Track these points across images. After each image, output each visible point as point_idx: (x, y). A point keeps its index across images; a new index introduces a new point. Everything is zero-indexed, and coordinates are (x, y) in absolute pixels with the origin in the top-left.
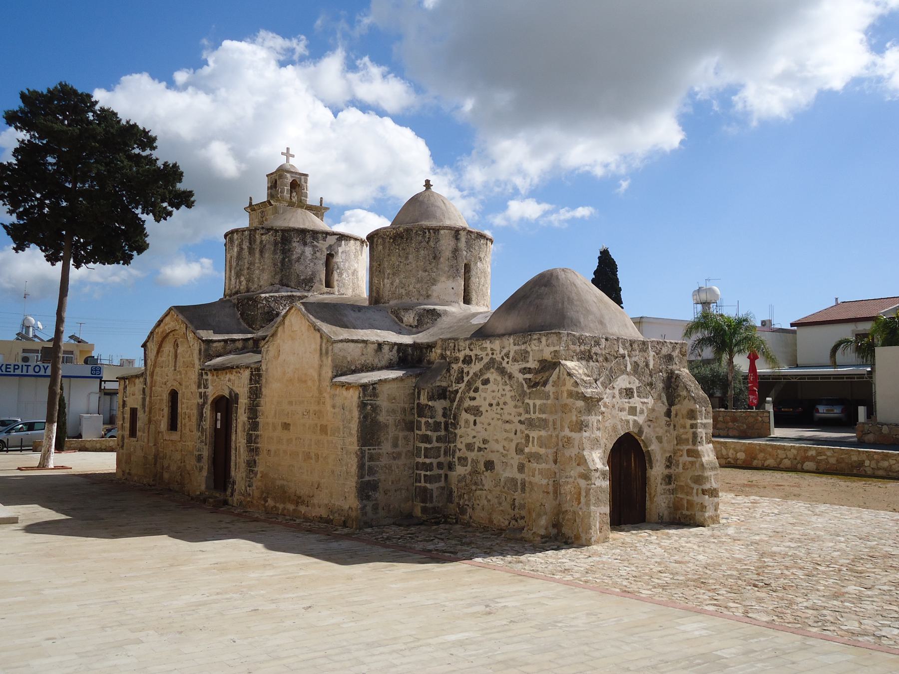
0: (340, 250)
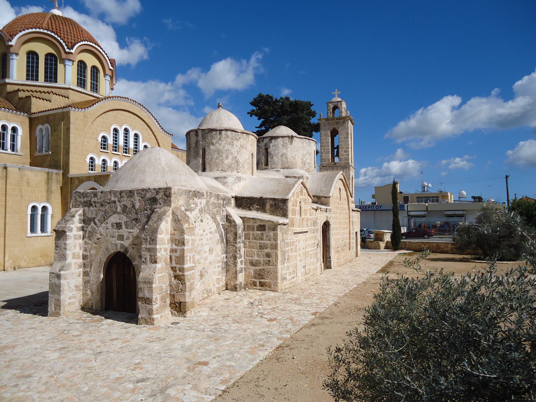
0: (271, 145)
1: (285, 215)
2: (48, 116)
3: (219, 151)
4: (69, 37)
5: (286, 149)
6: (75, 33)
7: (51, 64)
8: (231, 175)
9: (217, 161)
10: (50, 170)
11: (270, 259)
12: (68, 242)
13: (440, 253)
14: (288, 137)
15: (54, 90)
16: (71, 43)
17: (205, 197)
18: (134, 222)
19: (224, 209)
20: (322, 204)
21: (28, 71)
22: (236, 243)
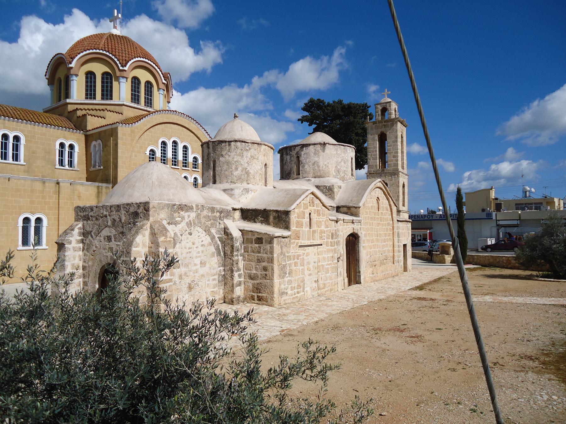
0: (303, 153)
1: (287, 228)
2: (100, 133)
3: (228, 163)
4: (124, 55)
5: (318, 157)
6: (130, 50)
7: (107, 83)
8: (238, 188)
9: (227, 173)
10: (100, 184)
11: (267, 273)
12: (66, 254)
13: (511, 268)
14: (320, 144)
15: (109, 108)
16: (125, 60)
17: (195, 210)
18: (121, 235)
19: (221, 222)
20: (352, 215)
21: (87, 90)
22: (233, 256)
